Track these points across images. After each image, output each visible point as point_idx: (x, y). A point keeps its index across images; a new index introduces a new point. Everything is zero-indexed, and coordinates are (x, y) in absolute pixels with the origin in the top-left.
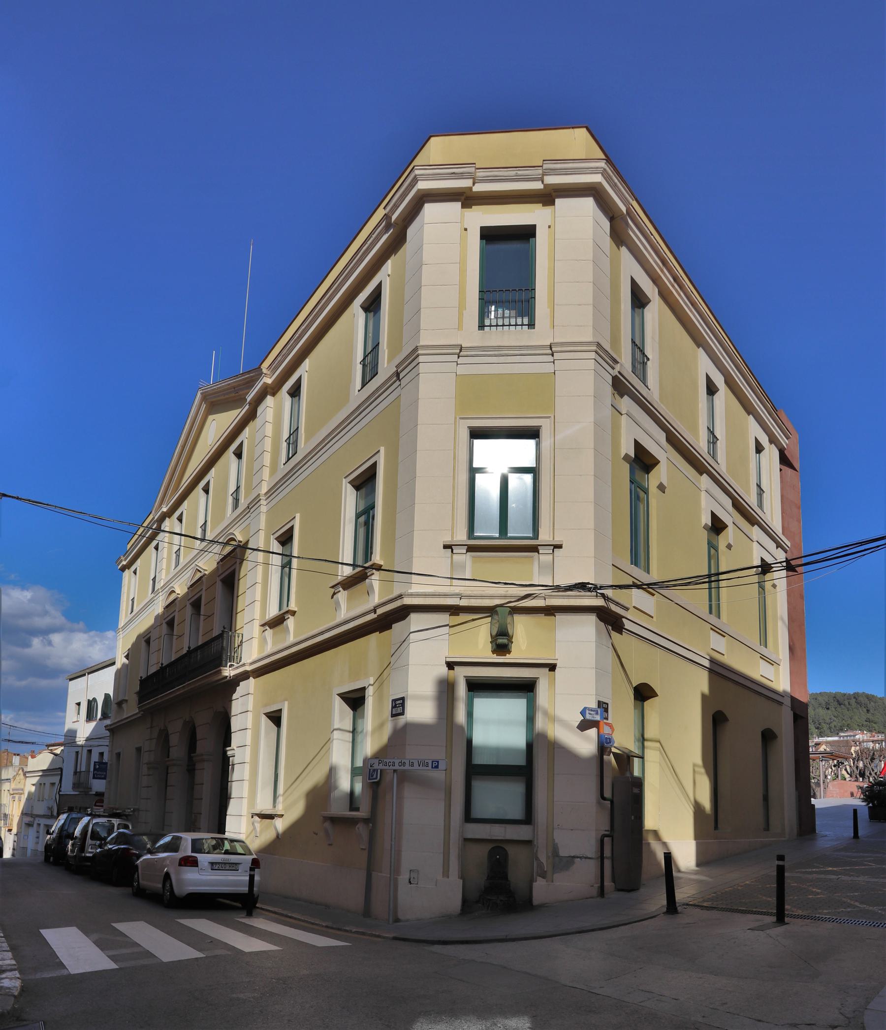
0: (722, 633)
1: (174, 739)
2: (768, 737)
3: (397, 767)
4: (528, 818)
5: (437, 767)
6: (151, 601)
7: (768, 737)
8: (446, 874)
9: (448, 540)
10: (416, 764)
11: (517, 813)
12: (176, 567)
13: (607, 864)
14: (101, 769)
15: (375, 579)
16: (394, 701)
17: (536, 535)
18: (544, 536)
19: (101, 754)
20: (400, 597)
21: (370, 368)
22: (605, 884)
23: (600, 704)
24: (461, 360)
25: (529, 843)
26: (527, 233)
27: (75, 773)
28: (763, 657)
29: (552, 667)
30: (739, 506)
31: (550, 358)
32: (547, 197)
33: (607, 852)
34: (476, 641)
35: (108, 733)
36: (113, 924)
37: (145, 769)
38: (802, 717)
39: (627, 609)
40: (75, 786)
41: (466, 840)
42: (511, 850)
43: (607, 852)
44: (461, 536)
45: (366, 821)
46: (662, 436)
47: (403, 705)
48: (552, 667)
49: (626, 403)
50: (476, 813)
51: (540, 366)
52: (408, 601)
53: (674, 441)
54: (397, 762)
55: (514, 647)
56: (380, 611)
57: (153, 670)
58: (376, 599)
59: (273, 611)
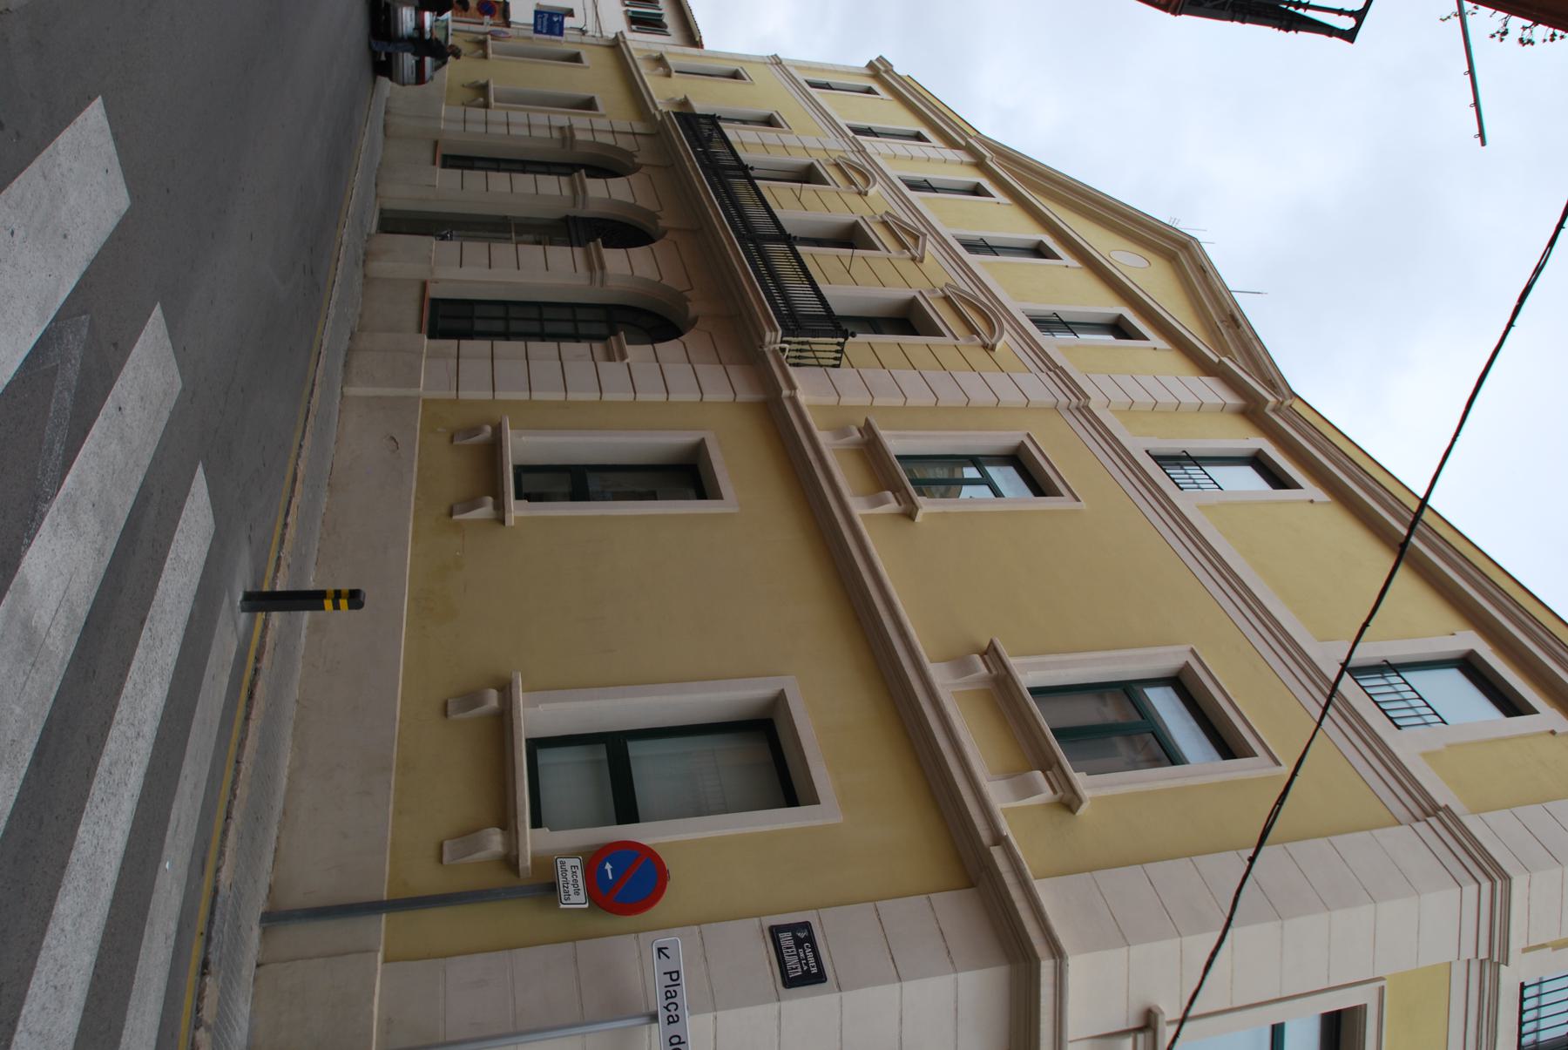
16: (806, 926)
20: (1057, 952)
37: (561, 119)
52: (1047, 967)
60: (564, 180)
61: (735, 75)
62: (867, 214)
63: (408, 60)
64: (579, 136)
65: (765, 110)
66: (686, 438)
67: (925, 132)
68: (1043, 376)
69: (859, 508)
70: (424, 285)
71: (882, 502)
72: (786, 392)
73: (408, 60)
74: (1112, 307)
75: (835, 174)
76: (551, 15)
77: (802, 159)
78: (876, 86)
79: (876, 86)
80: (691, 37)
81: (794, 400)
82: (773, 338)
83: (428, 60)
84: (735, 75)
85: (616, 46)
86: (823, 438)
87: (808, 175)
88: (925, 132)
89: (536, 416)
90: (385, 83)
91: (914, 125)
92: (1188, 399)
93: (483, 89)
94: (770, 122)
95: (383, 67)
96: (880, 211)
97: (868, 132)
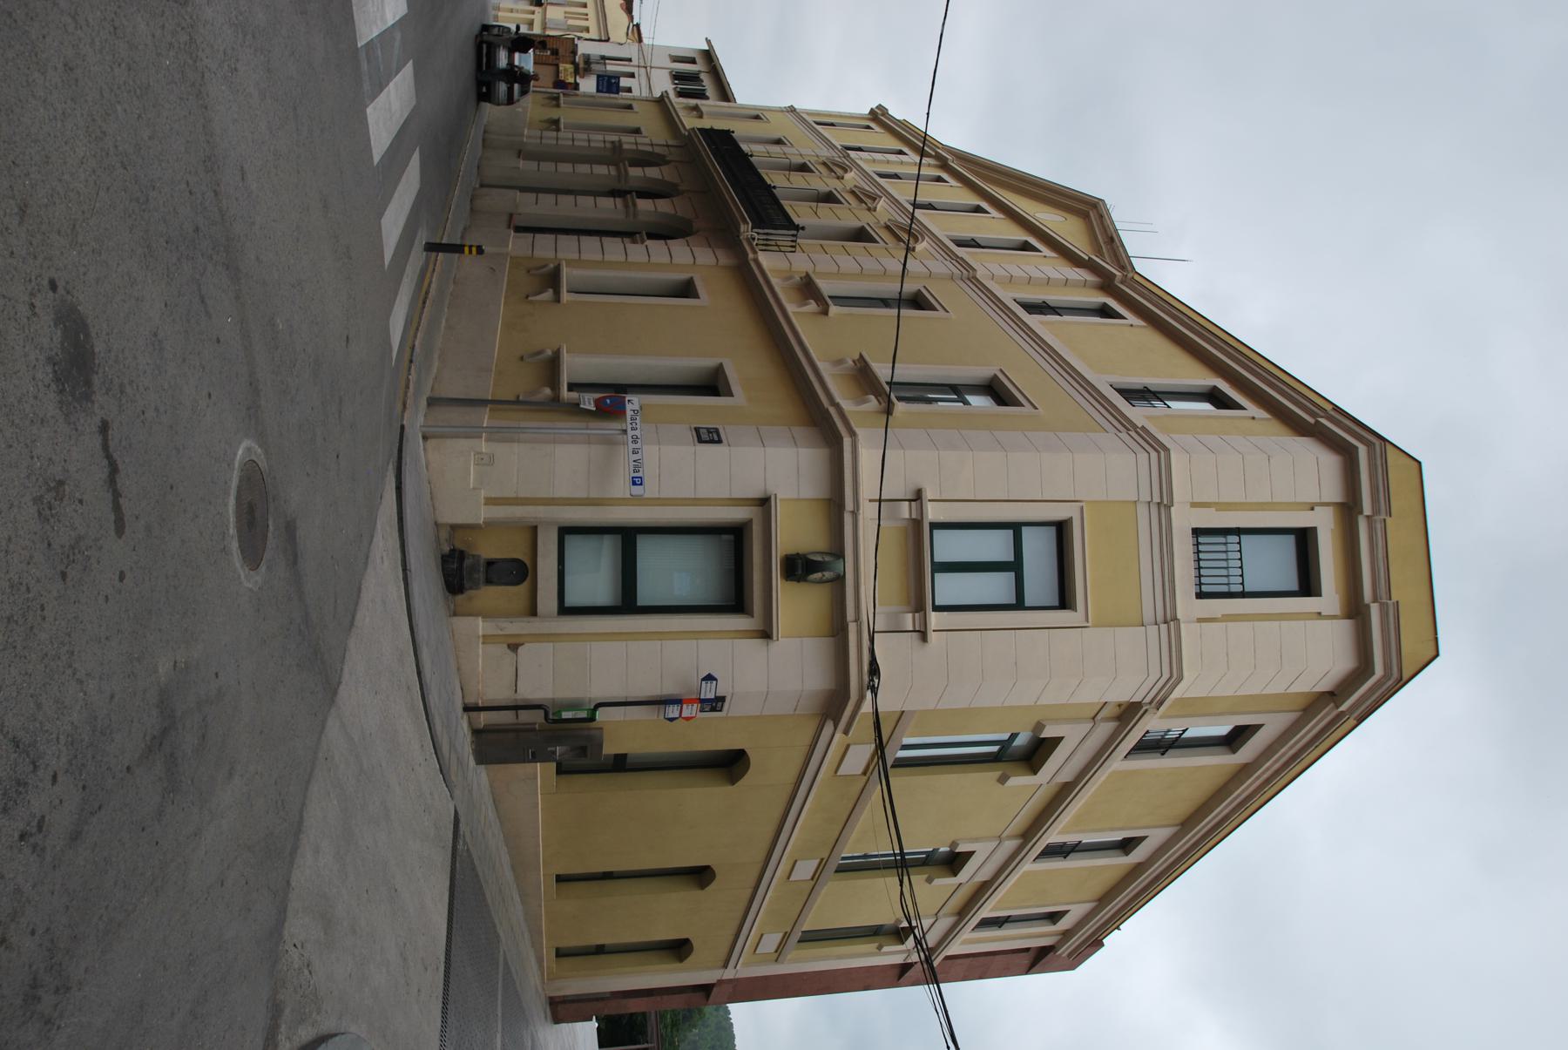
0: (816, 877)
1: (653, 172)
2: (679, 949)
3: (630, 433)
4: (565, 610)
5: (634, 483)
6: (833, 146)
7: (679, 949)
8: (490, 501)
9: (929, 494)
10: (636, 457)
11: (572, 599)
12: (882, 176)
13: (506, 718)
14: (609, 84)
15: (873, 403)
16: (717, 431)
17: (937, 609)
18: (935, 619)
19: (629, 90)
20: (853, 434)
21: (1136, 395)
22: (482, 714)
23: (722, 699)
24: (1154, 509)
25: (533, 612)
26: (1308, 585)
27: (604, 58)
28: (786, 936)
29: (766, 634)
30: (983, 890)
31: (1160, 617)
32: (1355, 610)
33: (525, 717)
34: (794, 531)
35: (657, 94)
36: (376, 159)
37: (615, 138)
38: (708, 996)
39: (846, 732)
40: (587, 59)
41: (534, 529)
42: (523, 588)
43: (525, 717)
44: (933, 513)
45: (556, 399)
46: (1066, 776)
47: (712, 441)
48: (766, 634)
49: (1105, 729)
50: (572, 542)
51: (1149, 606)
52: (847, 442)
53: (1063, 793)
54: (637, 433)
55: (793, 586)
56: (832, 410)
57: (744, 147)
58: (847, 406)
59: (826, 287)
60: (618, 200)
61: (757, 117)
62: (872, 221)
63: (502, 87)
64: (625, 146)
65: (776, 135)
66: (684, 276)
67: (985, 205)
68: (1124, 435)
69: (791, 308)
70: (511, 216)
71: (865, 402)
72: (751, 256)
73: (502, 87)
74: (1021, 236)
75: (885, 234)
76: (610, 77)
77: (800, 160)
78: (945, 176)
79: (945, 176)
80: (725, 94)
81: (756, 261)
82: (746, 230)
83: (516, 86)
84: (757, 117)
85: (662, 101)
86: (774, 281)
87: (803, 168)
88: (985, 205)
89: (578, 263)
90: (487, 107)
91: (1021, 236)
92: (1054, 275)
93: (556, 122)
94: (779, 142)
95: (484, 94)
96: (884, 220)
97: (972, 244)
